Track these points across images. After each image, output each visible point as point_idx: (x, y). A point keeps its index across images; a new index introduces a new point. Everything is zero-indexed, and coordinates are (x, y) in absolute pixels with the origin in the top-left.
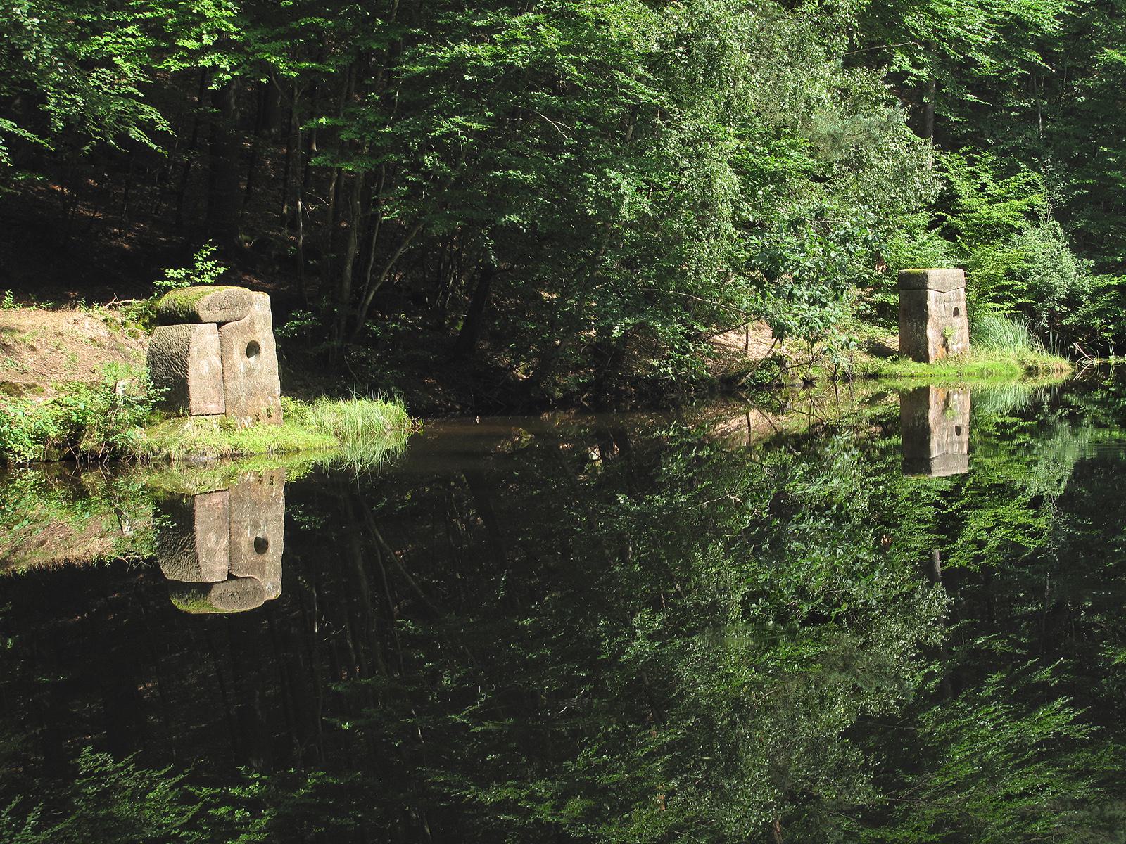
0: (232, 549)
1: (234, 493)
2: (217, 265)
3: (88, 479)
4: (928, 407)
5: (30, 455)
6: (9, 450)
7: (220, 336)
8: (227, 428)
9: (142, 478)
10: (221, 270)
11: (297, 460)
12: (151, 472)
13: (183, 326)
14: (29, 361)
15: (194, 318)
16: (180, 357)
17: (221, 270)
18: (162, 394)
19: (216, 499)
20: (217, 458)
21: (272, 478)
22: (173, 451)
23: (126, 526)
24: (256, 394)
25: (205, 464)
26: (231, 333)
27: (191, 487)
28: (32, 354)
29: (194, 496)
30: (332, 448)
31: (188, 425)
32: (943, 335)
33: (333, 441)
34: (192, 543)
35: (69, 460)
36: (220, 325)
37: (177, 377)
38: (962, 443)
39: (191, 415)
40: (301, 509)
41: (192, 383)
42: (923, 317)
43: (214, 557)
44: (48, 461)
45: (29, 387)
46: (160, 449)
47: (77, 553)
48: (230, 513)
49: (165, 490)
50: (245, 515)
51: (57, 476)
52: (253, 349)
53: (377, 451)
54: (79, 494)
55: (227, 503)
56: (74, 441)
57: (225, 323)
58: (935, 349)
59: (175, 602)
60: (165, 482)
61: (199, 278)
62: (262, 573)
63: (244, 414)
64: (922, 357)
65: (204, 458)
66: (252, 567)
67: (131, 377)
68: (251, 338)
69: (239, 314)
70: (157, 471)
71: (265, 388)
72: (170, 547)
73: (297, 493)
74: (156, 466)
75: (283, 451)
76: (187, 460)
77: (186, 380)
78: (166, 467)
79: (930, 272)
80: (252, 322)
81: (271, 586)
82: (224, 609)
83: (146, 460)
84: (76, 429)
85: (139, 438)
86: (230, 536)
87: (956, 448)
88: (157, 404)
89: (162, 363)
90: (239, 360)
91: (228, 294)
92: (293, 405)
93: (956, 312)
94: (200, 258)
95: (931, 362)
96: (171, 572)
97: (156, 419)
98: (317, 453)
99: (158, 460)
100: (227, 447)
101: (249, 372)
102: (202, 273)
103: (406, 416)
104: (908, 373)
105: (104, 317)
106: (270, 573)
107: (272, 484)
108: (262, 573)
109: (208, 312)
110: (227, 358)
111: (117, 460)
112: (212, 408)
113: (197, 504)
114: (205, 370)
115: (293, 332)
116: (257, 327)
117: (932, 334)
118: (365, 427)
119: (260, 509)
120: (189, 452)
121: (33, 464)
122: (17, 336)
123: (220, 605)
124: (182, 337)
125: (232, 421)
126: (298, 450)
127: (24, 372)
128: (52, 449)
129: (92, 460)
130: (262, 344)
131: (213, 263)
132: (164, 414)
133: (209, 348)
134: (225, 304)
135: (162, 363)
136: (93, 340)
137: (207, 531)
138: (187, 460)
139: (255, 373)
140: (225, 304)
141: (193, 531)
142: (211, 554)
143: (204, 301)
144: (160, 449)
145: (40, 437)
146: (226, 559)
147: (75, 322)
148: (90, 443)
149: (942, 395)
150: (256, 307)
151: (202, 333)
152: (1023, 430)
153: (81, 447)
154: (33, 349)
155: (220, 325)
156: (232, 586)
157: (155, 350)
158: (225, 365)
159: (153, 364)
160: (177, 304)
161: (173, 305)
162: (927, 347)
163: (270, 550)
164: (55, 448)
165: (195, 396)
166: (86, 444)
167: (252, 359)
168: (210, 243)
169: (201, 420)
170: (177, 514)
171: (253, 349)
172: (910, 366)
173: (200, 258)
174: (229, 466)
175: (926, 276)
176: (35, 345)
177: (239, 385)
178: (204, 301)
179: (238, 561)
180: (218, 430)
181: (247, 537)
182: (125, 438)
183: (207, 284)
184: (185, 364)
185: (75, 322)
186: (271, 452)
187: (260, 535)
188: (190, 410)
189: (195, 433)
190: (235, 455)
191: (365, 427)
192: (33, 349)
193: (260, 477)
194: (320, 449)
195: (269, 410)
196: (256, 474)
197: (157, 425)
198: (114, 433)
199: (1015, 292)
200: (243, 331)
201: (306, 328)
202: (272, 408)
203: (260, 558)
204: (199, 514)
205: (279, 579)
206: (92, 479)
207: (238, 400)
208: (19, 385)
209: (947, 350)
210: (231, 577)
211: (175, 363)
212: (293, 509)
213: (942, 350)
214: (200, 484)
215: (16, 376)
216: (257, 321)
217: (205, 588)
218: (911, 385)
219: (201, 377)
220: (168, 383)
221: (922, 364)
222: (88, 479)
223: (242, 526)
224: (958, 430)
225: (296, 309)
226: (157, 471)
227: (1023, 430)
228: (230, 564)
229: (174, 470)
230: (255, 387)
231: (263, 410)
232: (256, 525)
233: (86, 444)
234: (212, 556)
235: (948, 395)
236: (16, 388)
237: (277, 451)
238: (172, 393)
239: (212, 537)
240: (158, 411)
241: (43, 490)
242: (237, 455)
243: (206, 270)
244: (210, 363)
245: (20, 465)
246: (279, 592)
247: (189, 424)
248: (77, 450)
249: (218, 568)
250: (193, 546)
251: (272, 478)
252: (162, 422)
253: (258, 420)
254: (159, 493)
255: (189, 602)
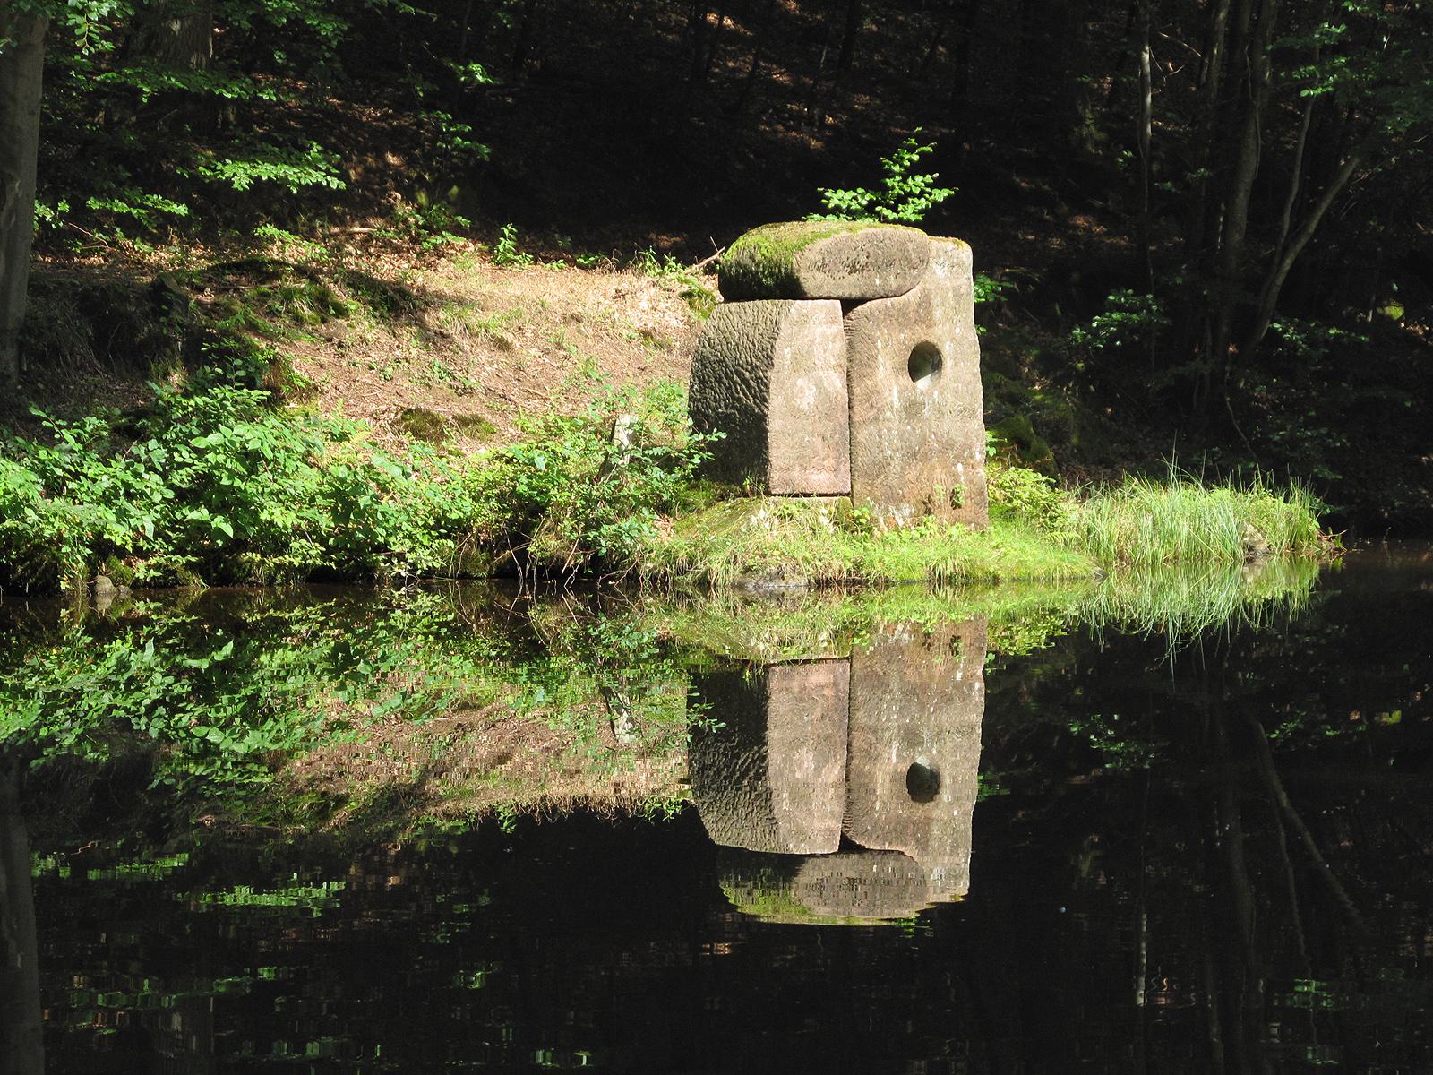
0: (853, 788)
1: (864, 668)
2: (937, 184)
3: (543, 618)
5: (426, 560)
6: (383, 548)
7: (849, 330)
8: (849, 525)
9: (656, 621)
10: (941, 195)
11: (995, 603)
12: (670, 609)
13: (768, 304)
14: (483, 367)
15: (788, 288)
16: (753, 368)
17: (941, 195)
18: (711, 446)
19: (818, 677)
20: (809, 586)
21: (955, 639)
22: (716, 566)
23: (622, 722)
24: (926, 458)
25: (780, 598)
26: (876, 323)
27: (762, 647)
28: (502, 357)
29: (768, 667)
30: (1074, 579)
31: (762, 514)
33: (1083, 563)
34: (759, 768)
35: (506, 577)
36: (849, 305)
37: (746, 411)
39: (768, 493)
40: (1112, 725)
41: (774, 425)
43: (808, 803)
44: (465, 577)
45: (463, 422)
46: (691, 561)
47: (596, 788)
48: (851, 711)
49: (709, 652)
50: (890, 716)
51: (482, 609)
52: (923, 360)
53: (1221, 598)
54: (527, 649)
55: (844, 685)
56: (518, 534)
57: (862, 301)
59: (731, 893)
60: (713, 629)
61: (895, 209)
62: (923, 845)
63: (896, 499)
65: (774, 586)
66: (900, 829)
67: (659, 410)
68: (920, 335)
69: (893, 283)
70: (682, 609)
71: (947, 446)
72: (718, 773)
73: (1006, 677)
74: (682, 596)
75: (966, 581)
76: (740, 586)
77: (762, 418)
78: (702, 600)
80: (925, 303)
81: (946, 874)
82: (823, 914)
83: (660, 583)
84: (527, 513)
85: (654, 538)
86: (849, 759)
88: (705, 465)
89: (719, 381)
90: (889, 380)
91: (870, 239)
92: (1028, 482)
94: (897, 168)
96: (724, 830)
97: (698, 498)
98: (1040, 588)
99: (683, 584)
100: (836, 565)
101: (912, 409)
102: (903, 199)
103: (1314, 526)
105: (685, 288)
106: (942, 844)
107: (955, 651)
108: (923, 845)
109: (820, 276)
110: (862, 377)
111: (602, 580)
112: (820, 480)
113: (774, 684)
114: (807, 398)
115: (1113, 337)
116: (938, 313)
118: (1215, 546)
119: (923, 706)
120: (747, 569)
121: (427, 580)
122: (474, 318)
123: (808, 906)
124: (761, 326)
125: (862, 512)
126: (996, 581)
127: (466, 392)
128: (475, 552)
129: (551, 577)
130: (947, 349)
131: (929, 178)
132: (717, 489)
133: (818, 351)
134: (863, 260)
135: (719, 381)
136: (646, 334)
137: (795, 744)
138: (740, 586)
139: (926, 412)
140: (863, 260)
141: (762, 741)
142: (800, 795)
143: (813, 254)
144: (691, 561)
145: (446, 527)
146: (838, 808)
147: (619, 295)
148: (552, 542)
150: (938, 270)
151: (804, 320)
153: (531, 549)
154: (503, 345)
155: (849, 305)
156: (850, 866)
157: (707, 352)
158: (857, 390)
159: (702, 381)
160: (758, 257)
161: (752, 257)
163: (945, 795)
164: (482, 549)
165: (779, 453)
166: (543, 544)
167: (924, 383)
168: (917, 137)
169: (792, 506)
170: (732, 706)
171: (923, 360)
173: (897, 168)
174: (839, 607)
176: (508, 337)
177: (886, 436)
178: (813, 254)
179: (871, 813)
180: (831, 529)
181: (890, 764)
182: (618, 536)
183: (908, 223)
184: (763, 383)
185: (619, 295)
186: (938, 581)
187: (922, 760)
188: (766, 483)
189: (768, 533)
190: (854, 582)
191: (1215, 546)
192: (503, 345)
193: (927, 635)
194: (1048, 580)
195: (954, 493)
196: (916, 628)
197: (699, 512)
198: (597, 524)
200: (902, 319)
201: (1134, 330)
202: (963, 488)
203: (919, 811)
204: (778, 706)
205: (964, 860)
206: (552, 619)
207: (881, 468)
208: (442, 417)
210: (847, 846)
211: (744, 381)
212: (1094, 725)
214: (781, 643)
215: (446, 399)
216: (936, 301)
217: (786, 867)
219: (796, 413)
220: (724, 422)
222: (543, 618)
223: (879, 739)
225: (1118, 284)
226: (682, 609)
228: (848, 817)
229: (716, 605)
230: (924, 441)
231: (940, 491)
232: (911, 739)
233: (543, 544)
234: (803, 798)
236: (435, 422)
237: (951, 580)
238: (732, 446)
239: (806, 759)
240: (704, 482)
241: (453, 634)
242: (856, 583)
243: (911, 194)
244: (819, 386)
245: (399, 582)
246: (962, 888)
247: (762, 513)
248: (523, 555)
249: (817, 824)
250: (761, 774)
251: (955, 639)
252: (709, 505)
253: (928, 512)
254: (697, 658)
255: (757, 893)
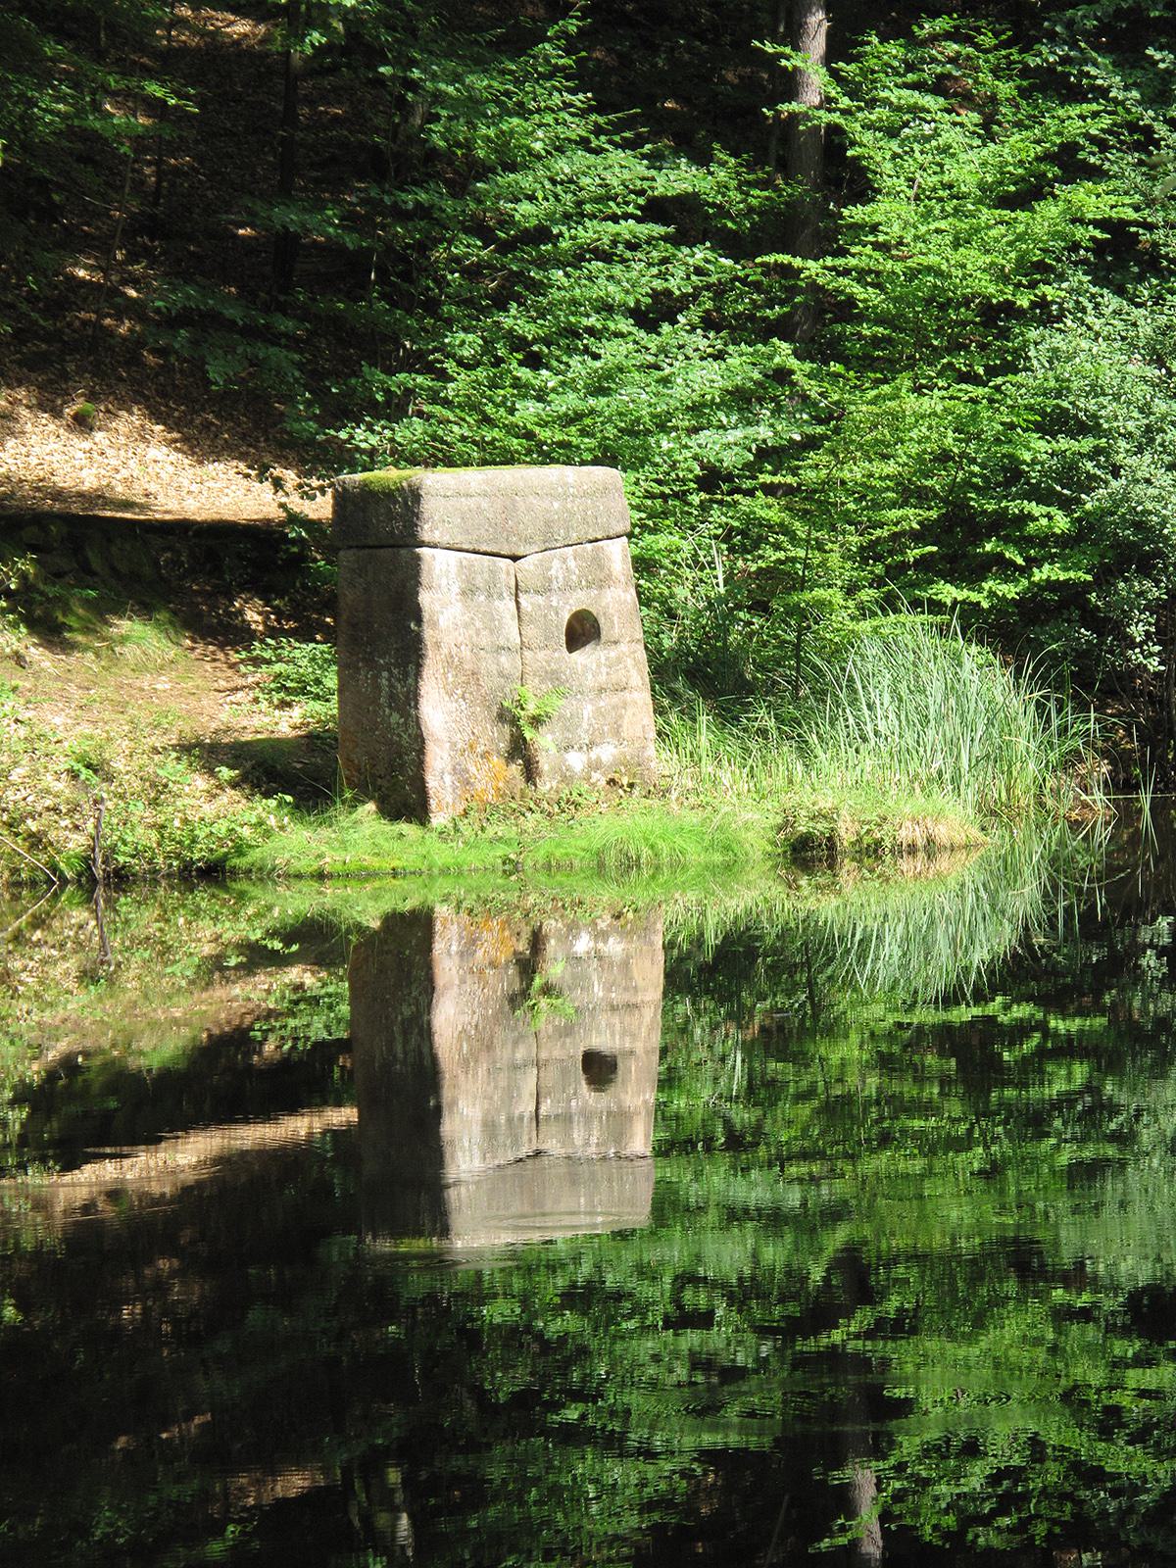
4: (428, 987)
32: (505, 717)
38: (620, 1120)
42: (409, 653)
58: (459, 771)
64: (406, 801)
79: (435, 482)
87: (586, 1140)
93: (582, 631)
95: (438, 820)
104: (342, 862)
117: (442, 713)
136: (616, 643)
149: (499, 945)
152: (1067, 1049)
162: (420, 765)
172: (361, 832)
175: (414, 495)
199: (1024, 542)
209: (530, 773)
213: (496, 774)
218: (368, 911)
221: (404, 827)
224: (599, 1068)
227: (1067, 1049)
235: (537, 941)
